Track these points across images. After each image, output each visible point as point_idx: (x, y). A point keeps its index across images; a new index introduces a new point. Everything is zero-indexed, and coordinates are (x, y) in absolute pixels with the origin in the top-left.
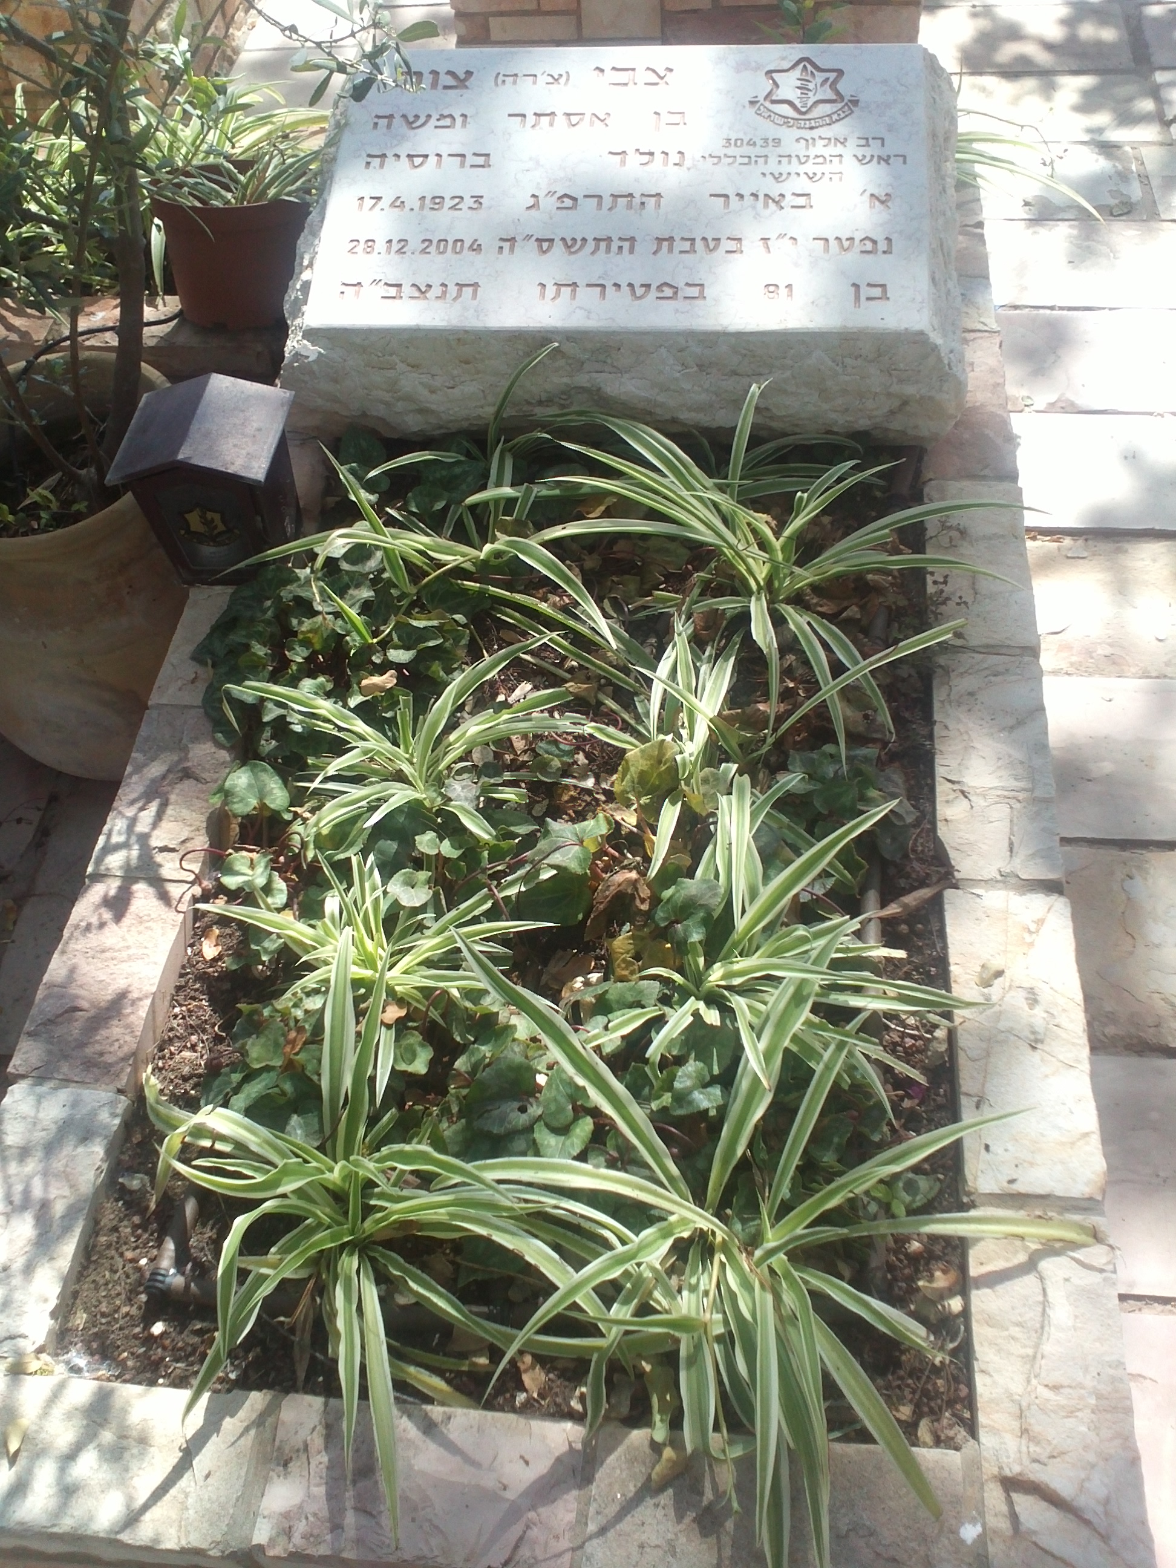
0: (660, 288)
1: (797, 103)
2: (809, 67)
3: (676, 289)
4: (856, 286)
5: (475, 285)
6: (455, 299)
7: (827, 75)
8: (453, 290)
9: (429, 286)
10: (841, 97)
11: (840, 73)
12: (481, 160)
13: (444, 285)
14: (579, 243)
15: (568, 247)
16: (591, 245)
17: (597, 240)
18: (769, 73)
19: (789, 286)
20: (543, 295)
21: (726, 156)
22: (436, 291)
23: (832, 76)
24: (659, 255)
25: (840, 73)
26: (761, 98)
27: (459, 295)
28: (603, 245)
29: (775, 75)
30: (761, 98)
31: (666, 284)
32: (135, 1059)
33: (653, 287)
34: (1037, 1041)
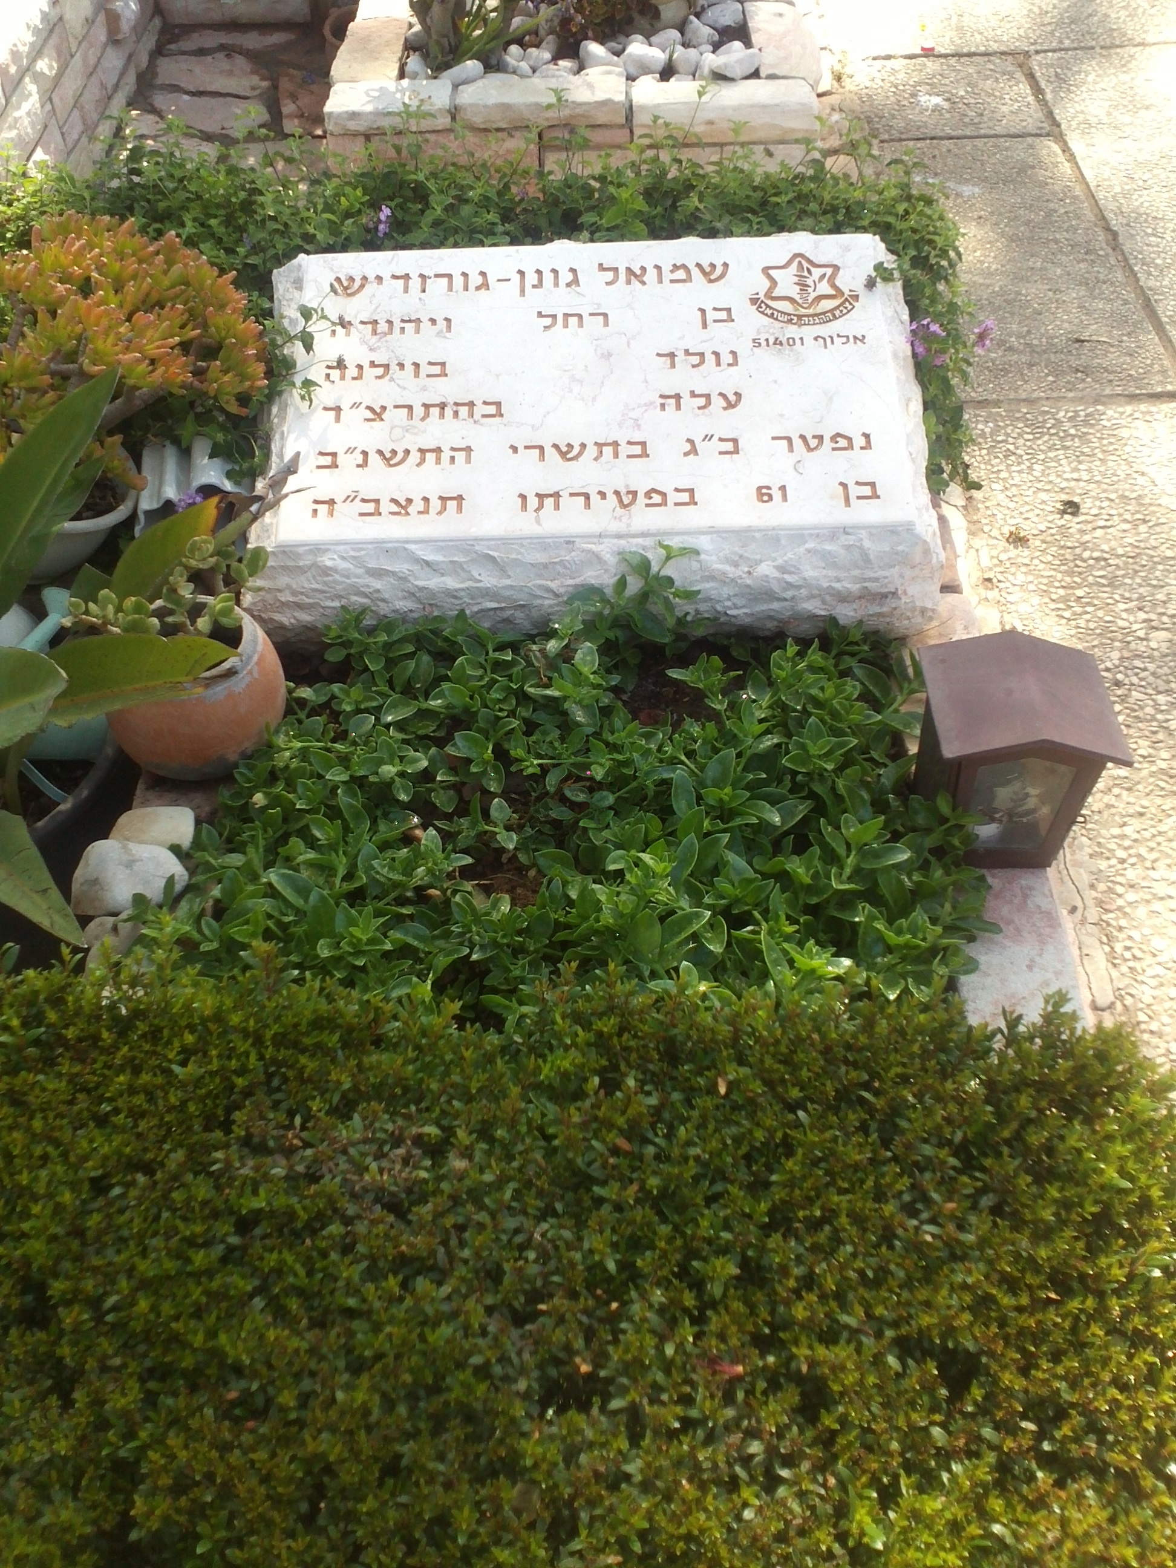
0: (648, 495)
1: (797, 298)
2: (805, 265)
3: (664, 495)
4: (844, 486)
5: (460, 498)
6: (440, 513)
7: (822, 271)
8: (435, 504)
9: (409, 501)
10: (839, 292)
11: (836, 268)
12: (437, 370)
13: (426, 500)
14: (400, 456)
15: (563, 455)
16: (591, 451)
17: (600, 445)
18: (766, 270)
19: (783, 488)
20: (524, 507)
21: (373, 364)
22: (419, 505)
23: (829, 271)
24: (603, 459)
25: (836, 268)
26: (761, 296)
27: (444, 508)
28: (608, 451)
29: (771, 272)
30: (761, 296)
31: (654, 491)
32: (504, 1231)
33: (641, 496)
34: (488, 1274)
